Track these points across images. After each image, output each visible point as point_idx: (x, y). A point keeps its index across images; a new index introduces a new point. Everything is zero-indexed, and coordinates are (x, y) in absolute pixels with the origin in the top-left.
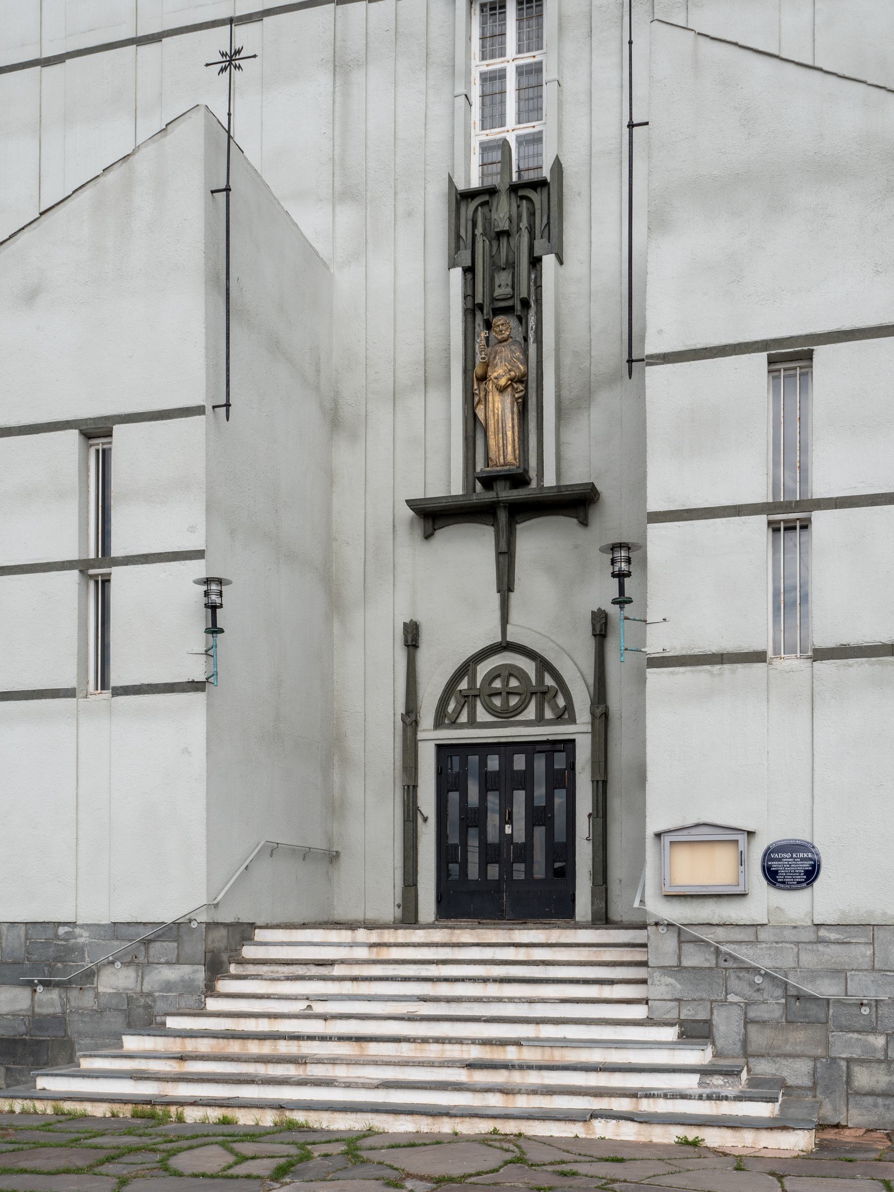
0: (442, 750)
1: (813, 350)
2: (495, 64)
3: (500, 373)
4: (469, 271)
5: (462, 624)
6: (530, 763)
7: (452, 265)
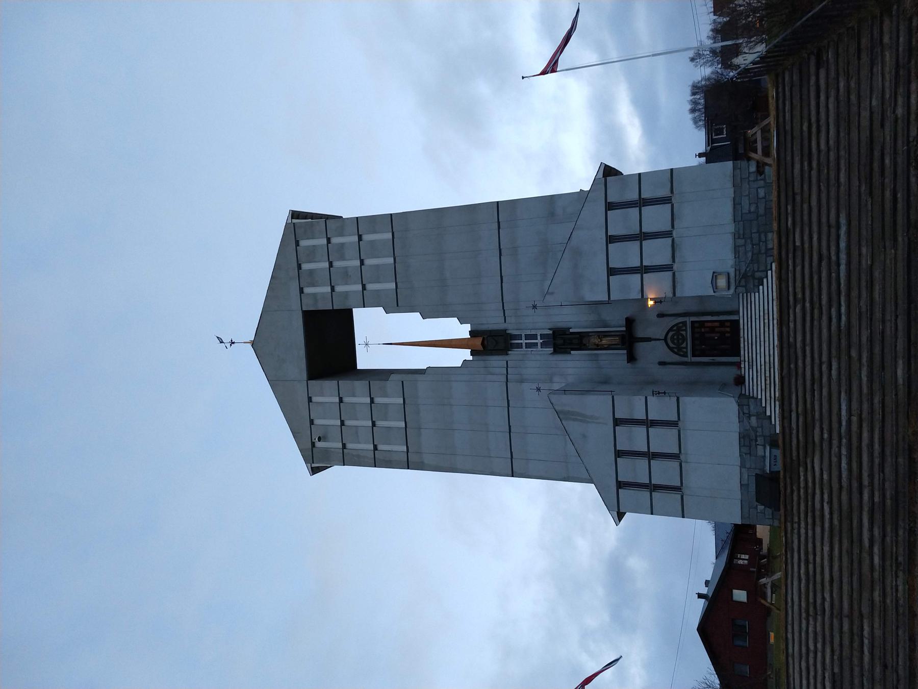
0: (694, 355)
3: (597, 341)
5: (660, 351)
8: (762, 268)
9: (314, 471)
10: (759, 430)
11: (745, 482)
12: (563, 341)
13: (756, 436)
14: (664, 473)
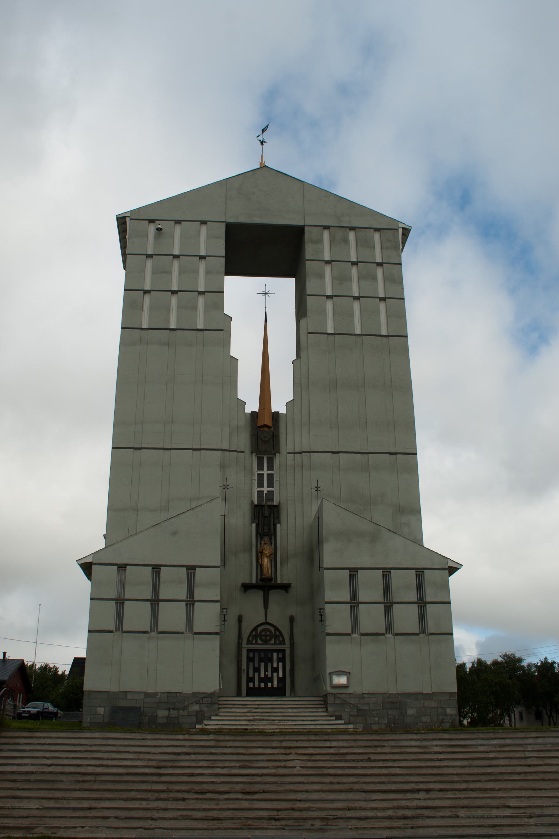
0: (249, 651)
4: (257, 525)
6: (254, 655)
7: (253, 522)
9: (122, 221)
10: (186, 713)
11: (129, 697)
12: (266, 516)
13: (178, 709)
14: (137, 615)
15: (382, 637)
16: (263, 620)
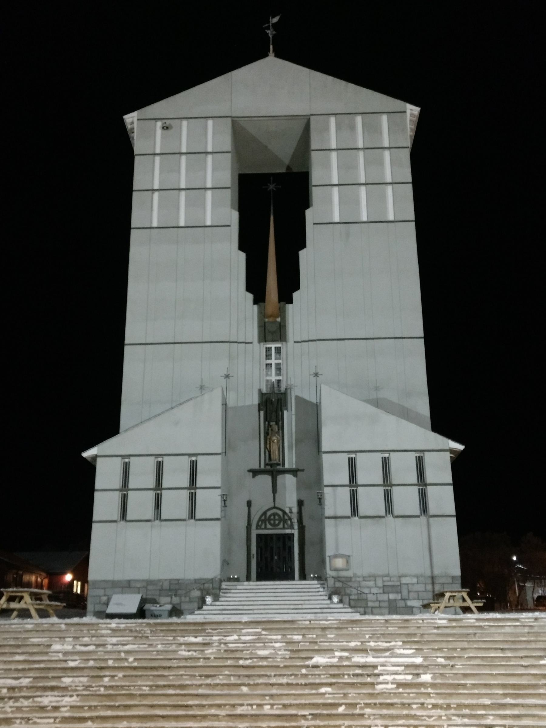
1: (297, 398)
2: (269, 362)
8: (352, 603)
10: (187, 599)
11: (133, 584)
13: (180, 596)
15: (383, 520)
16: (272, 505)
